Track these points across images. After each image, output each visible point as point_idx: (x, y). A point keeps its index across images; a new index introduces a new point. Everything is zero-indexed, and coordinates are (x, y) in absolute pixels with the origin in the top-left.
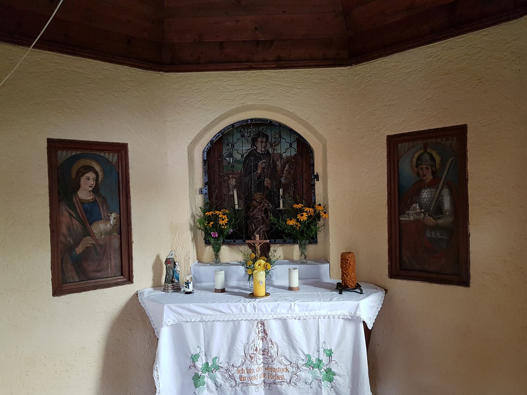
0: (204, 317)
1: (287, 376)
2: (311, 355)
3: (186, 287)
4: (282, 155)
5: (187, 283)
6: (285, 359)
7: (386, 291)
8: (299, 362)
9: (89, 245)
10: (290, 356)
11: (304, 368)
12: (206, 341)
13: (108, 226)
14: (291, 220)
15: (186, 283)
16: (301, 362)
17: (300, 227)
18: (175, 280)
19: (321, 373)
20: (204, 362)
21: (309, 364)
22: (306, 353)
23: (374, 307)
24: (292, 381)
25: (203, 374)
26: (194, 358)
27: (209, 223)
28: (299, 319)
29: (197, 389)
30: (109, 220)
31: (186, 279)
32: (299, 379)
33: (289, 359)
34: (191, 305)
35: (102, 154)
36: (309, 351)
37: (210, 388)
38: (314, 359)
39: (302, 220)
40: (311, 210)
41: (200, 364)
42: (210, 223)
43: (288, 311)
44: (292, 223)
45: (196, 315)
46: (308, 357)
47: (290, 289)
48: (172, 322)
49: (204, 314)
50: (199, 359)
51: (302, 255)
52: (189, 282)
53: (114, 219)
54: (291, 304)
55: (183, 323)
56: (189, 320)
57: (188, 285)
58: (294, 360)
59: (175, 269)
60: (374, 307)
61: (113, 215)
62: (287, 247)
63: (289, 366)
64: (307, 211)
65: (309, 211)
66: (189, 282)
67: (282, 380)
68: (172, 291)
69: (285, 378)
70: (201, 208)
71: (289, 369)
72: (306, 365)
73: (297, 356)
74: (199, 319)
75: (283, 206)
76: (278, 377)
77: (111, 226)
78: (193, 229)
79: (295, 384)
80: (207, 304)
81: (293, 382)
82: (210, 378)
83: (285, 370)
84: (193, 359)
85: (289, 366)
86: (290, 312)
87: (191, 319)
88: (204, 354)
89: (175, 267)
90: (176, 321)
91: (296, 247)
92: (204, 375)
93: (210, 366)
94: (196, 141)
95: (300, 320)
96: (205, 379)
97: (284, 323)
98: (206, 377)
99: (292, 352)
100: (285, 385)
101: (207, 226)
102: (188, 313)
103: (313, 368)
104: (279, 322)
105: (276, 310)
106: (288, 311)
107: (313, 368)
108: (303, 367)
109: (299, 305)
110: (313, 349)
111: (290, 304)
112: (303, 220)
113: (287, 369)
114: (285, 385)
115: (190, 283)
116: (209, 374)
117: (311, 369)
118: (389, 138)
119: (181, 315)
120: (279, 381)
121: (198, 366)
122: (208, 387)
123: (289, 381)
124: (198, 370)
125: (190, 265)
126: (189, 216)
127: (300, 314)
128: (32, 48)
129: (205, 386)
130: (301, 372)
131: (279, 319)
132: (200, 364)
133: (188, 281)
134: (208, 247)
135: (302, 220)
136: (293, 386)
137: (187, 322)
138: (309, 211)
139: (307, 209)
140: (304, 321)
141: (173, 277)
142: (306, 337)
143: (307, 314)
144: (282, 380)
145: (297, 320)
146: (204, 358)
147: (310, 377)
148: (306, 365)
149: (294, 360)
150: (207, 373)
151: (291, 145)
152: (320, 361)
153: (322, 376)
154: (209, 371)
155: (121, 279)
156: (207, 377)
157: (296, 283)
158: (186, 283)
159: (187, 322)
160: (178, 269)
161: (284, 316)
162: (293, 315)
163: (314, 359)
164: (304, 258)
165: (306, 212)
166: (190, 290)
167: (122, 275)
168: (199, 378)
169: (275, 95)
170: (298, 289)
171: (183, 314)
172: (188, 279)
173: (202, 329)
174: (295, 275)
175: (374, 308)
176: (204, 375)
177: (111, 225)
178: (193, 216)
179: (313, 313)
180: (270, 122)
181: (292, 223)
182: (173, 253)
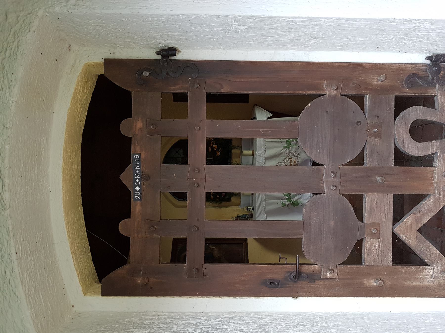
0: (263, 199)
1: (294, 158)
2: (284, 146)
3: (250, 210)
4: (182, 157)
5: (248, 209)
6: (286, 159)
7: (256, 105)
8: (287, 152)
9: (225, 259)
10: (284, 156)
11: (290, 149)
12: (276, 199)
13: (216, 249)
14: (217, 154)
15: (248, 210)
16: (287, 151)
17: (221, 149)
18: (246, 216)
19: (293, 141)
20: (286, 200)
21: (288, 147)
22: (283, 148)
23: (262, 112)
24: (296, 156)
25: (292, 201)
26: (283, 205)
27: (217, 198)
28: (265, 151)
29: (299, 204)
30: (213, 249)
31: (245, 210)
32: (296, 152)
33: (285, 157)
34: (256, 206)
35: (178, 251)
36: (282, 147)
37: (299, 198)
38: (286, 144)
39: (217, 148)
40: (212, 142)
41: (287, 203)
42: (139, 146)
43: (261, 157)
44: (218, 153)
45: (261, 203)
46: (285, 147)
47: (253, 155)
48: (265, 216)
49: (261, 200)
50: (284, 203)
51: (237, 148)
52: (247, 208)
53: (212, 246)
54: (258, 155)
55: (266, 210)
56: (264, 207)
57: (249, 209)
58: (286, 154)
59: (241, 216)
60: (262, 112)
61: (210, 247)
62: (233, 156)
63: (289, 157)
64: (212, 145)
65: (212, 143)
66: (247, 208)
67: (296, 161)
68: (252, 218)
69: (295, 159)
70: (210, 203)
71: (291, 157)
72: (289, 149)
73: (284, 153)
74: (264, 202)
75: (212, 157)
76: (295, 163)
77: (216, 248)
78: (221, 207)
79: (298, 154)
80: (257, 198)
81: (297, 155)
82: (294, 197)
83: (291, 159)
84: (284, 206)
85: (289, 157)
86: (261, 156)
87: (264, 206)
88: (281, 200)
89: (240, 216)
90: (264, 214)
91: (233, 151)
92: (292, 200)
93: (287, 197)
94: (173, 204)
95: (266, 150)
96: (295, 200)
97: (267, 159)
98: (294, 200)
99: (282, 155)
100: (299, 160)
101: (219, 199)
102: (260, 208)
103: (291, 145)
104: (266, 161)
105: (260, 163)
106: (261, 157)
107: (291, 145)
108: (290, 150)
109: (258, 151)
110: (281, 145)
111: (258, 156)
112: (217, 147)
113: (291, 158)
114: (299, 160)
115: (248, 208)
116: (292, 198)
117: (291, 146)
118: (174, 101)
119: (261, 211)
120: (296, 162)
121: (288, 203)
122: (298, 199)
123: (297, 158)
124: (290, 203)
125: (240, 209)
126: (213, 209)
127: (262, 151)
128: (127, 258)
129: (298, 200)
130: (293, 151)
131: (265, 161)
132: (287, 203)
133: (247, 209)
134: (232, 200)
135: (217, 148)
136: (299, 156)
137: (265, 208)
138: (212, 143)
139: (211, 145)
140: (266, 149)
141: (245, 217)
142: (275, 148)
143: (263, 147)
144: (296, 161)
145: (266, 152)
146: (284, 200)
147: (295, 147)
148: (289, 149)
149: (286, 155)
150: (292, 199)
151: (177, 152)
152: (287, 142)
153: (294, 141)
154: (291, 198)
155: (244, 244)
156: (294, 199)
157: (250, 152)
158: (248, 210)
159: (265, 208)
160: (241, 214)
161: (263, 159)
162: (263, 155)
163: (286, 144)
164: (238, 147)
165: (213, 145)
166: (251, 208)
167: (242, 244)
168: (294, 203)
169: (9, 289)
170: (253, 151)
171: (261, 210)
172: (245, 209)
173: (269, 201)
174: (245, 152)
175: (262, 112)
176: (292, 200)
177: (215, 248)
178: (214, 207)
179: (263, 144)
180: (248, 219)
181: (218, 153)
182: (232, 217)
